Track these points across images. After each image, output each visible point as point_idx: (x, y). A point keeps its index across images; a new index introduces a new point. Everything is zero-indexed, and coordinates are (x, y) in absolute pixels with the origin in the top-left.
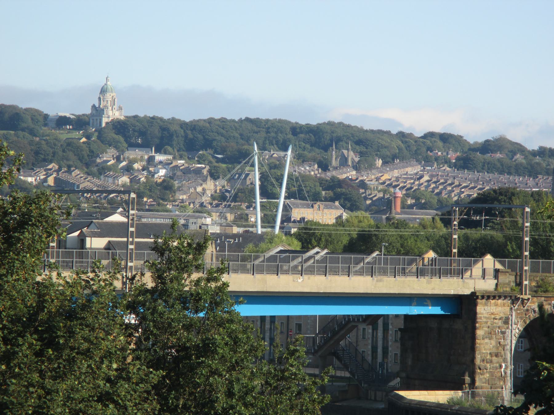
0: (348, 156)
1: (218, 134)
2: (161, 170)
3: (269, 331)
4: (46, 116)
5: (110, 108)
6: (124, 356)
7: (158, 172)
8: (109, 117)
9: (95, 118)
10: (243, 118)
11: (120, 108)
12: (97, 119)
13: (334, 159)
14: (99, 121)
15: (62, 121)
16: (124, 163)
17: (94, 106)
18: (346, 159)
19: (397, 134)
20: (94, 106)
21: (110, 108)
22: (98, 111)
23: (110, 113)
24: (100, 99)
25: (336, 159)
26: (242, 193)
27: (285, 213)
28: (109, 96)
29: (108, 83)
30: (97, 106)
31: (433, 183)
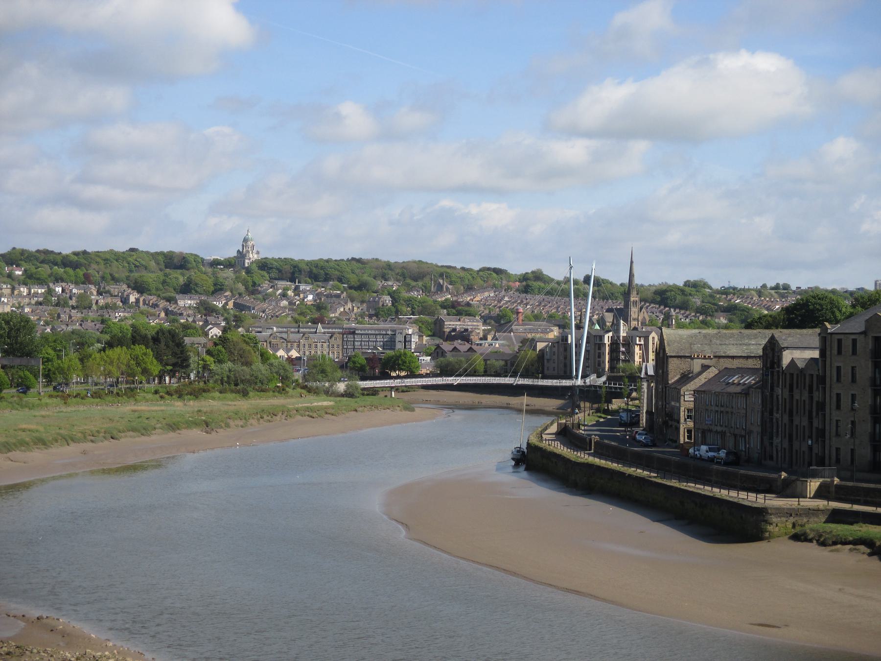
0: (443, 284)
1: (335, 269)
2: (309, 296)
3: (780, 452)
4: (203, 260)
5: (251, 252)
6: (798, 529)
7: (307, 297)
8: (250, 259)
9: (240, 259)
10: (350, 258)
11: (258, 253)
12: (241, 261)
13: (433, 286)
14: (242, 261)
15: (215, 263)
16: (280, 291)
17: (238, 251)
18: (442, 286)
19: (461, 268)
20: (238, 251)
21: (251, 252)
22: (241, 255)
23: (251, 256)
24: (243, 245)
25: (434, 286)
26: (382, 311)
27: (596, 288)
28: (250, 244)
29: (249, 234)
30: (241, 251)
31: (498, 307)
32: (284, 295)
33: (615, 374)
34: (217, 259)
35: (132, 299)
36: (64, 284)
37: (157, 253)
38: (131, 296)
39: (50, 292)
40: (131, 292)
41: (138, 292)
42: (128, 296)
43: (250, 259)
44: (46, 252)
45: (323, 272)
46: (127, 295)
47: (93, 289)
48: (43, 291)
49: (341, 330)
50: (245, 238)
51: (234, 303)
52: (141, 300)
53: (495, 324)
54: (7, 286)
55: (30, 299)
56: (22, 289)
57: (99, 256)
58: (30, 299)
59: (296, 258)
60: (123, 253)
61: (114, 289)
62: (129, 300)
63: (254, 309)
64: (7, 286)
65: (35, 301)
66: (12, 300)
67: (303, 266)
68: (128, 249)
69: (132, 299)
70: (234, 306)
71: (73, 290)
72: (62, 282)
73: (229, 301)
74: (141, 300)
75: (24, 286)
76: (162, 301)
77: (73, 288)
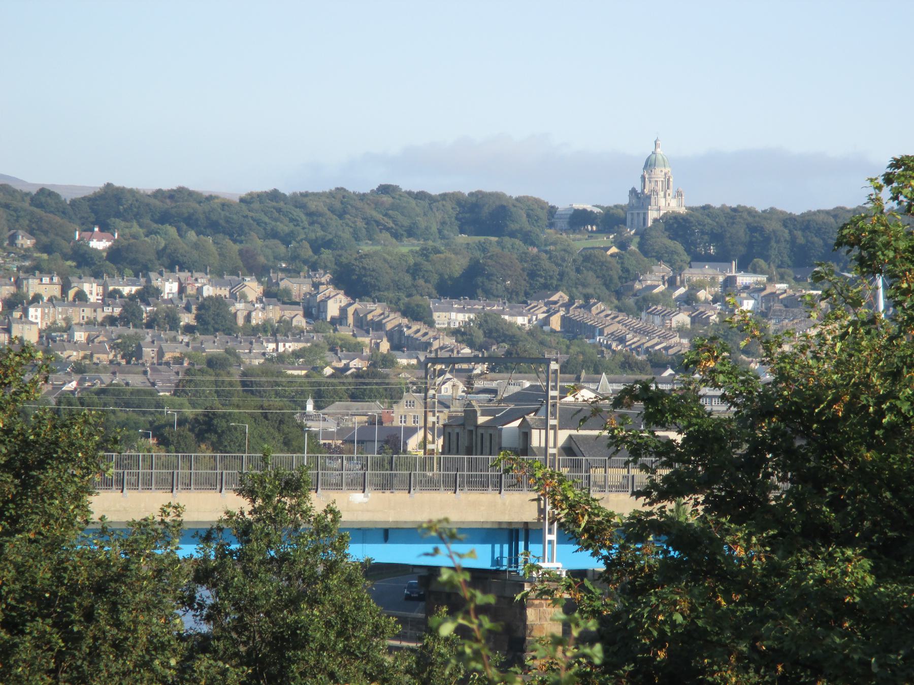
4: (552, 211)
5: (662, 194)
7: (741, 304)
9: (635, 212)
11: (679, 194)
12: (638, 214)
14: (641, 216)
16: (682, 291)
17: (633, 192)
20: (633, 192)
22: (641, 200)
23: (662, 203)
24: (643, 178)
28: (659, 173)
30: (639, 191)
32: (689, 300)
33: (603, 458)
34: (585, 210)
35: (333, 310)
36: (184, 275)
37: (444, 196)
38: (330, 303)
39: (149, 294)
40: (332, 294)
41: (347, 294)
42: (324, 302)
43: (659, 210)
44: (179, 195)
45: (821, 242)
46: (322, 301)
47: (253, 288)
48: (134, 289)
49: (456, 366)
50: (649, 158)
51: (563, 318)
52: (351, 310)
53: (121, 288)
54: (51, 279)
55: (95, 311)
56: (86, 287)
57: (302, 206)
58: (95, 311)
59: (760, 205)
60: (363, 197)
61: (299, 287)
62: (325, 312)
63: (601, 333)
64: (51, 279)
65: (104, 315)
66: (54, 312)
67: (772, 226)
68: (375, 187)
69: (333, 310)
70: (563, 325)
71: (205, 288)
72: (180, 270)
73: (551, 315)
74: (351, 310)
75: (92, 279)
76: (392, 316)
77: (205, 285)
